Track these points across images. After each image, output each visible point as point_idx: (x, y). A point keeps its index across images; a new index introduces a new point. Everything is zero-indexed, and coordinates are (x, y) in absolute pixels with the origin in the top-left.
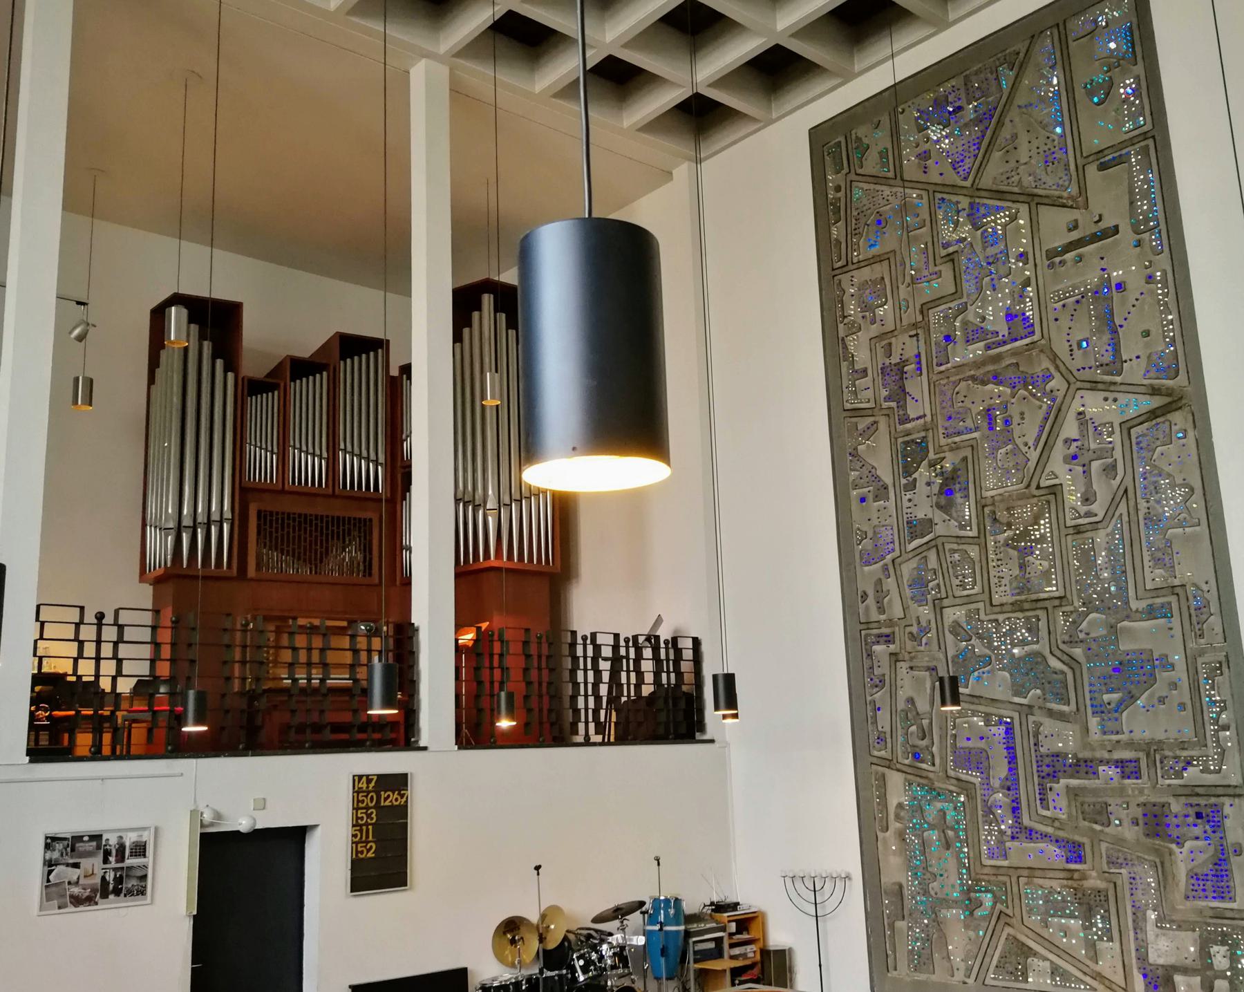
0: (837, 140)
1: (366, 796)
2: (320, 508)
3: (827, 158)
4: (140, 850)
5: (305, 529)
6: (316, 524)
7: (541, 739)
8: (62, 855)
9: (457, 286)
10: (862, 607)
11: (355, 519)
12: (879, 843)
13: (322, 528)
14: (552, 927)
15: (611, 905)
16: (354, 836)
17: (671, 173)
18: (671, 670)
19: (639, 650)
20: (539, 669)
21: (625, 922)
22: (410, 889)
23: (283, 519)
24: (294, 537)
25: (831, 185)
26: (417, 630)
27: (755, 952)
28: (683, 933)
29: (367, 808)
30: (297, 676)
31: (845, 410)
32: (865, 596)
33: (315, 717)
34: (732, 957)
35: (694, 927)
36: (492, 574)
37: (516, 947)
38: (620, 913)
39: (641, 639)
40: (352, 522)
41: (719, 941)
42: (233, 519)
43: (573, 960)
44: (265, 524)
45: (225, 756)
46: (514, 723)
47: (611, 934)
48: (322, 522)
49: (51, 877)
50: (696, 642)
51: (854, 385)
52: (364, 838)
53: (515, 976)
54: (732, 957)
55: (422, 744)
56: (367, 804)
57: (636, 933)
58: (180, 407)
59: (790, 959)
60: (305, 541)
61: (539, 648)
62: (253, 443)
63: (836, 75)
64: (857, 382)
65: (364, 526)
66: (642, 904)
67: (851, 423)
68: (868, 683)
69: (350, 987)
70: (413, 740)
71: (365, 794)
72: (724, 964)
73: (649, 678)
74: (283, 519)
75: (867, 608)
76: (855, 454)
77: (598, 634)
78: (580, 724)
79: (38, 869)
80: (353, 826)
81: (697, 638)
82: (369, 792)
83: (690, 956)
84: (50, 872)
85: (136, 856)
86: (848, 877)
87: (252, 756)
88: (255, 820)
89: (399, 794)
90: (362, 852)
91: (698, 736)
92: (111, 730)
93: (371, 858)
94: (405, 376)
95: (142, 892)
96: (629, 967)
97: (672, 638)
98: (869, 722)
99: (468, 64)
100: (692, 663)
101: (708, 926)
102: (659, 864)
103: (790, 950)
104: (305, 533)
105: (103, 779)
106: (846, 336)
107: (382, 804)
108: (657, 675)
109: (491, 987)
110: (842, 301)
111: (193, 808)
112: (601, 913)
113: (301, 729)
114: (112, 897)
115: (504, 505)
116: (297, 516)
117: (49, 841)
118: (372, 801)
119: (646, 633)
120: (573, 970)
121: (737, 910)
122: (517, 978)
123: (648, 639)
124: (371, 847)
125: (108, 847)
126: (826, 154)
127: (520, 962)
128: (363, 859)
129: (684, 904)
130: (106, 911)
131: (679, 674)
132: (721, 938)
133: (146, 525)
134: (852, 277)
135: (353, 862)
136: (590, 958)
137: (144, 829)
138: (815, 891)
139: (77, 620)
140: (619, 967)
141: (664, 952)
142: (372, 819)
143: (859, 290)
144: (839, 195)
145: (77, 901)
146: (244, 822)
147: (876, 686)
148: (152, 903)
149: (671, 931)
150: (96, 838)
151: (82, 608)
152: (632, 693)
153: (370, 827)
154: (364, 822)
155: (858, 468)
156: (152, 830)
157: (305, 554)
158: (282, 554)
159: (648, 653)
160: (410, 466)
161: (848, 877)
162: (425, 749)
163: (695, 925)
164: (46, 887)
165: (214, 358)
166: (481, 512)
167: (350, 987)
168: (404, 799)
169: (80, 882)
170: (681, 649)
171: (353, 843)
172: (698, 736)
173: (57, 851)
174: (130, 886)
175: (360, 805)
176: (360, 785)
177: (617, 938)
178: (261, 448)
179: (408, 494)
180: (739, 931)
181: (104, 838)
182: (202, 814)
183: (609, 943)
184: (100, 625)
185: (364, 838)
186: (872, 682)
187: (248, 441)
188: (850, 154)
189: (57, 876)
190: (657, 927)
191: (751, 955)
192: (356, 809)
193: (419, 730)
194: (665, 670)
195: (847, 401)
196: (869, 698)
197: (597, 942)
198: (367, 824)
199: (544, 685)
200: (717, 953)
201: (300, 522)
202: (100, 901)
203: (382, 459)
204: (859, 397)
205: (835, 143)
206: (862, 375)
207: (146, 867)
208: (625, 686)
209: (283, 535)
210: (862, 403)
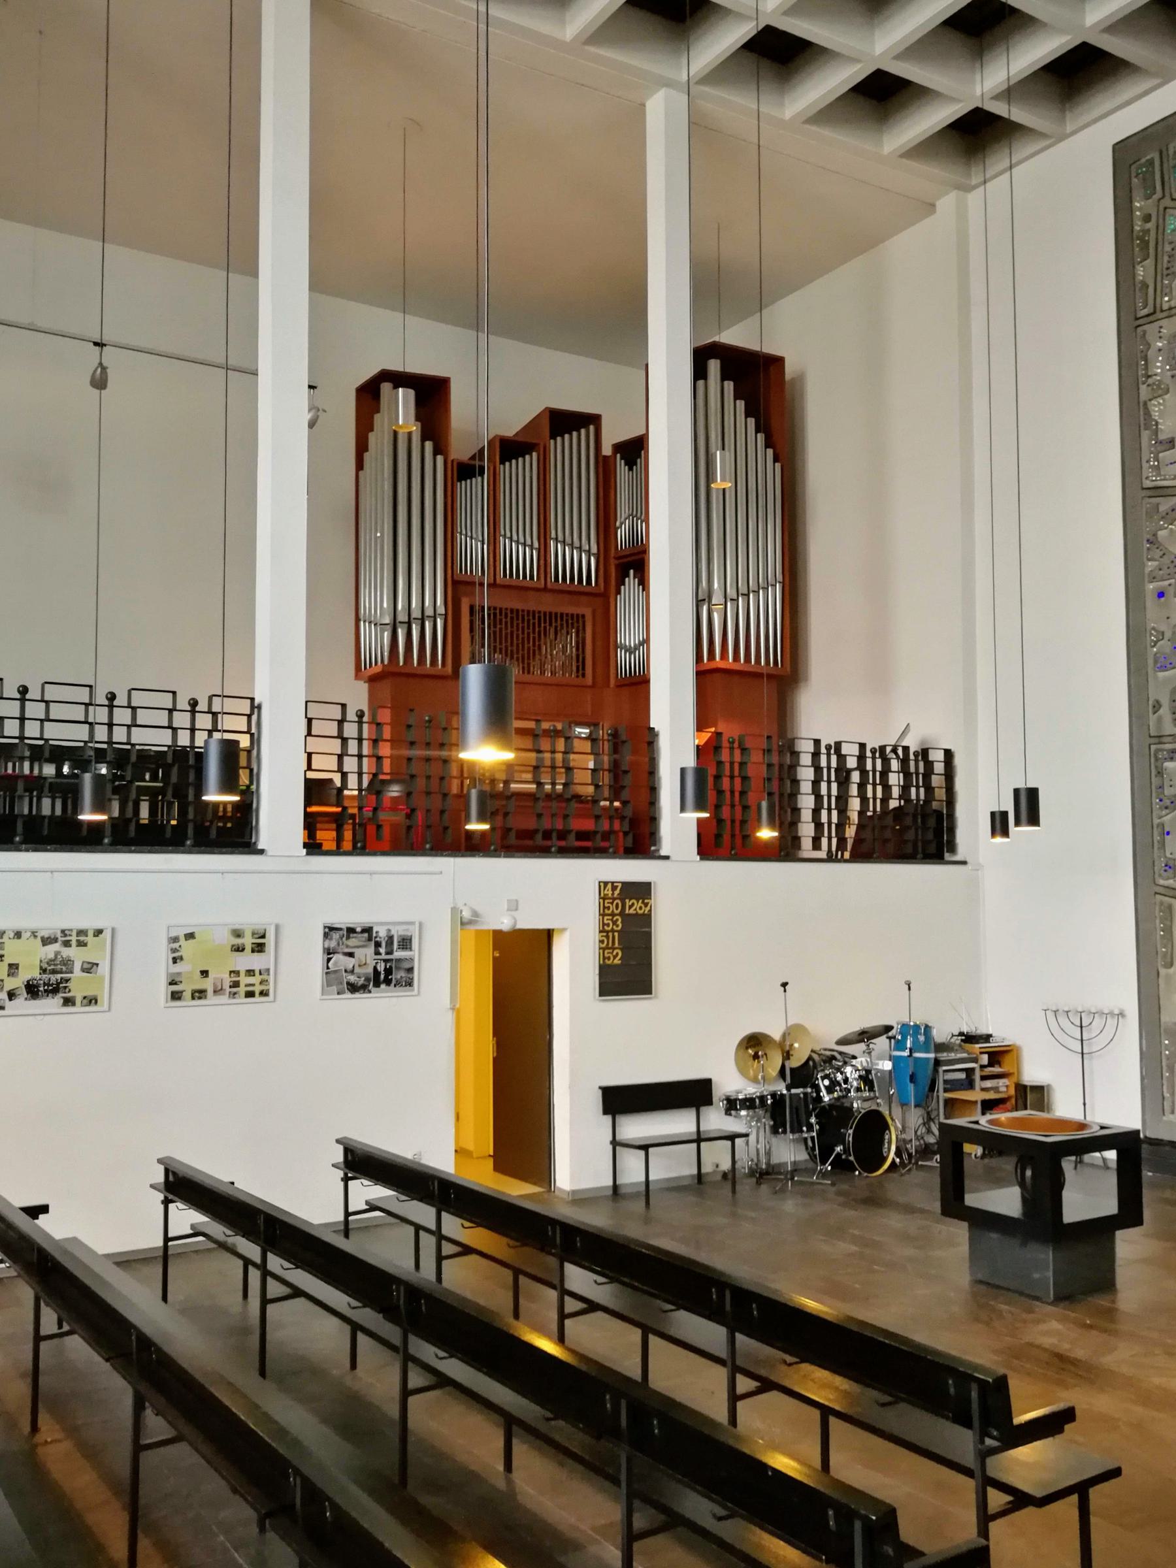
0: (1148, 157)
1: (612, 903)
2: (532, 604)
3: (1135, 181)
4: (406, 943)
5: (518, 624)
7: (733, 852)
8: (338, 944)
10: (1153, 719)
11: (567, 615)
12: (1160, 980)
13: (534, 624)
14: (796, 1045)
15: (856, 1027)
16: (601, 942)
17: (933, 205)
18: (921, 784)
19: (886, 762)
21: (871, 1046)
22: (656, 997)
25: (1138, 213)
27: (1007, 1086)
28: (933, 1061)
29: (613, 915)
30: (542, 781)
31: (1143, 489)
32: (1157, 706)
33: (559, 825)
34: (983, 1089)
35: (944, 1056)
36: (717, 676)
37: (759, 1062)
38: (866, 1036)
39: (889, 749)
40: (537, 615)
41: (970, 1072)
42: (446, 615)
43: (818, 1079)
47: (854, 1057)
49: (330, 964)
50: (949, 755)
51: (1156, 459)
52: (610, 945)
53: (760, 1090)
54: (983, 1089)
55: (663, 853)
56: (613, 911)
57: (881, 1058)
58: (391, 494)
59: (1048, 1100)
61: (732, 754)
62: (464, 532)
63: (1155, 75)
64: (1161, 455)
65: (577, 621)
66: (888, 1028)
67: (1150, 503)
68: (1157, 803)
69: (600, 1088)
71: (611, 901)
72: (976, 1095)
73: (896, 792)
75: (1160, 720)
76: (1153, 541)
77: (843, 744)
78: (823, 839)
79: (319, 957)
80: (600, 932)
81: (950, 750)
82: (614, 899)
83: (940, 1085)
84: (329, 960)
85: (403, 948)
86: (1122, 1014)
87: (505, 857)
88: (515, 919)
89: (643, 902)
90: (609, 958)
91: (947, 856)
92: (334, 826)
93: (617, 965)
95: (410, 984)
96: (875, 1091)
97: (739, 736)
98: (1156, 848)
99: (841, 138)
100: (943, 777)
101: (960, 1056)
102: (909, 989)
103: (1049, 1086)
104: (518, 630)
105: (222, 873)
106: (1150, 400)
107: (627, 912)
108: (905, 789)
109: (736, 1100)
110: (1146, 356)
111: (452, 906)
112: (847, 1035)
113: (547, 835)
114: (383, 986)
115: (731, 600)
117: (327, 930)
118: (617, 908)
119: (893, 743)
120: (818, 1091)
121: (989, 1042)
122: (762, 1092)
123: (894, 750)
124: (617, 954)
125: (378, 939)
126: (1133, 174)
127: (763, 1078)
128: (609, 965)
129: (935, 1032)
130: (383, 999)
131: (929, 789)
132: (973, 1069)
133: (360, 620)
134: (1161, 327)
135: (601, 967)
136: (836, 1079)
137: (412, 923)
138: (1081, 1027)
139: (339, 718)
140: (865, 1090)
141: (913, 1078)
142: (617, 926)
143: (1169, 343)
144: (1149, 226)
145: (353, 988)
146: (505, 921)
147: (1166, 808)
148: (274, 1001)
149: (919, 1058)
150: (368, 930)
151: (344, 706)
152: (878, 809)
153: (616, 934)
154: (610, 928)
155: (1157, 557)
156: (417, 925)
157: (518, 653)
158: (495, 652)
159: (895, 765)
161: (1122, 1014)
162: (667, 858)
163: (945, 1054)
164: (327, 973)
166: (705, 608)
167: (600, 1088)
168: (648, 908)
169: (355, 971)
170: (845, 756)
171: (600, 949)
172: (947, 856)
173: (334, 940)
174: (399, 977)
175: (606, 911)
176: (606, 892)
177: (861, 1061)
178: (518, 542)
180: (991, 1064)
181: (375, 930)
182: (461, 911)
183: (852, 1066)
184: (111, 707)
185: (610, 945)
186: (1161, 803)
187: (502, 533)
188: (1165, 172)
189: (336, 964)
190: (906, 1053)
191: (1004, 1089)
192: (602, 915)
193: (660, 839)
194: (914, 784)
195: (1147, 478)
196: (1156, 821)
197: (840, 1064)
198: (613, 931)
199: (737, 794)
200: (969, 1084)
201: (512, 618)
202: (373, 990)
203: (594, 550)
204: (1162, 473)
205: (1147, 161)
206: (1167, 446)
207: (412, 960)
208: (871, 801)
210: (1164, 480)
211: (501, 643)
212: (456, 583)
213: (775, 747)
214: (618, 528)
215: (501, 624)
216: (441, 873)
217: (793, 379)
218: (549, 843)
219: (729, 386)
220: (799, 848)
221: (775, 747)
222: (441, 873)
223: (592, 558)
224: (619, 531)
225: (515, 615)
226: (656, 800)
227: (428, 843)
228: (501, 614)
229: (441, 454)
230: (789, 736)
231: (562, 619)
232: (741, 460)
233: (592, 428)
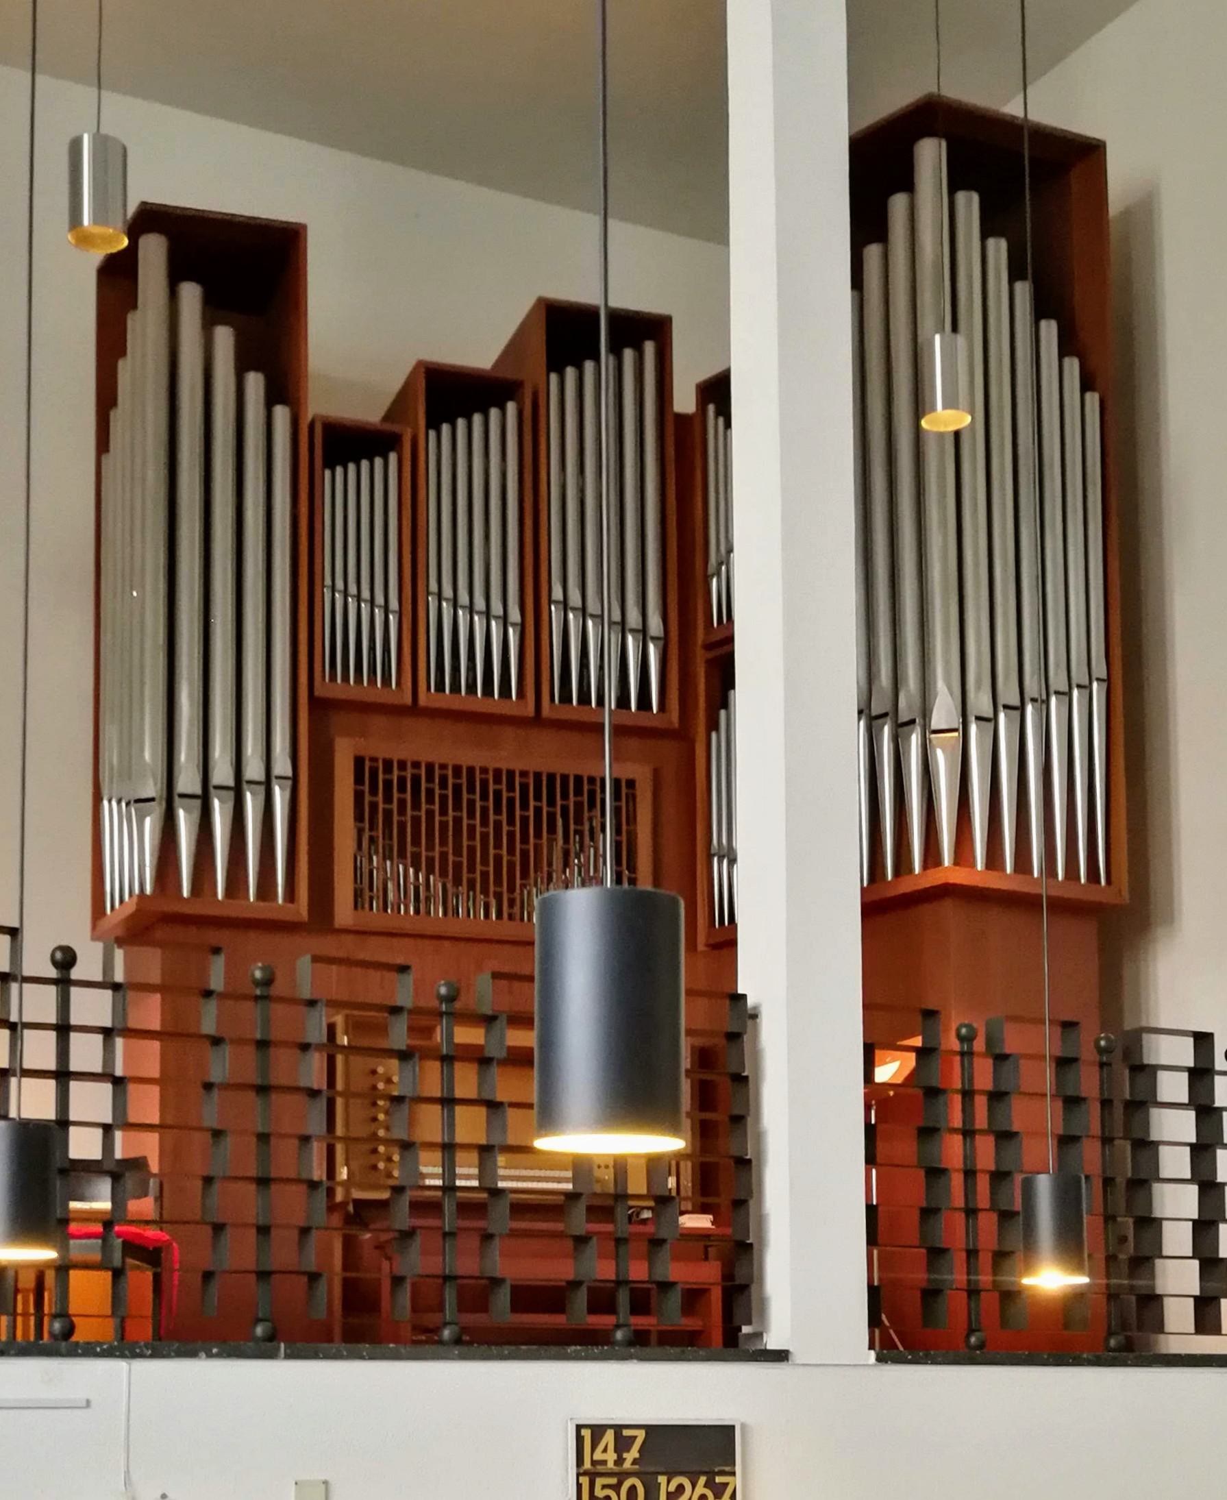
1: (617, 1488)
5: (471, 804)
6: (498, 794)
9: (856, 129)
13: (511, 801)
20: (971, 1212)
23: (416, 780)
24: (444, 826)
26: (754, 1016)
36: (948, 907)
42: (295, 779)
44: (373, 791)
45: (210, 1355)
46: (1083, 1280)
48: (511, 788)
55: (772, 1342)
60: (471, 836)
70: (746, 1329)
71: (613, 1481)
74: (416, 780)
82: (622, 1476)
87: (290, 1356)
89: (709, 1484)
94: (711, 408)
113: (602, 1301)
115: (978, 718)
116: (450, 773)
133: (102, 800)
157: (471, 869)
160: (730, 640)
162: (781, 1356)
165: (242, 368)
166: (915, 740)
176: (598, 1456)
179: (723, 713)
187: (433, 587)
193: (763, 1302)
201: (457, 789)
209: (416, 821)
211: (430, 847)
212: (320, 706)
213: (1088, 1054)
214: (713, 576)
215: (430, 800)
216: (88, 1404)
217: (1127, 213)
218: (606, 1320)
219: (969, 204)
220: (1159, 1327)
221: (1088, 1054)
222: (88, 1404)
223: (652, 648)
224: (715, 580)
225: (464, 781)
226: (750, 1193)
227: (258, 1320)
228: (430, 778)
229: (283, 402)
230: (1128, 1025)
231: (578, 792)
232: (1000, 397)
233: (649, 347)
